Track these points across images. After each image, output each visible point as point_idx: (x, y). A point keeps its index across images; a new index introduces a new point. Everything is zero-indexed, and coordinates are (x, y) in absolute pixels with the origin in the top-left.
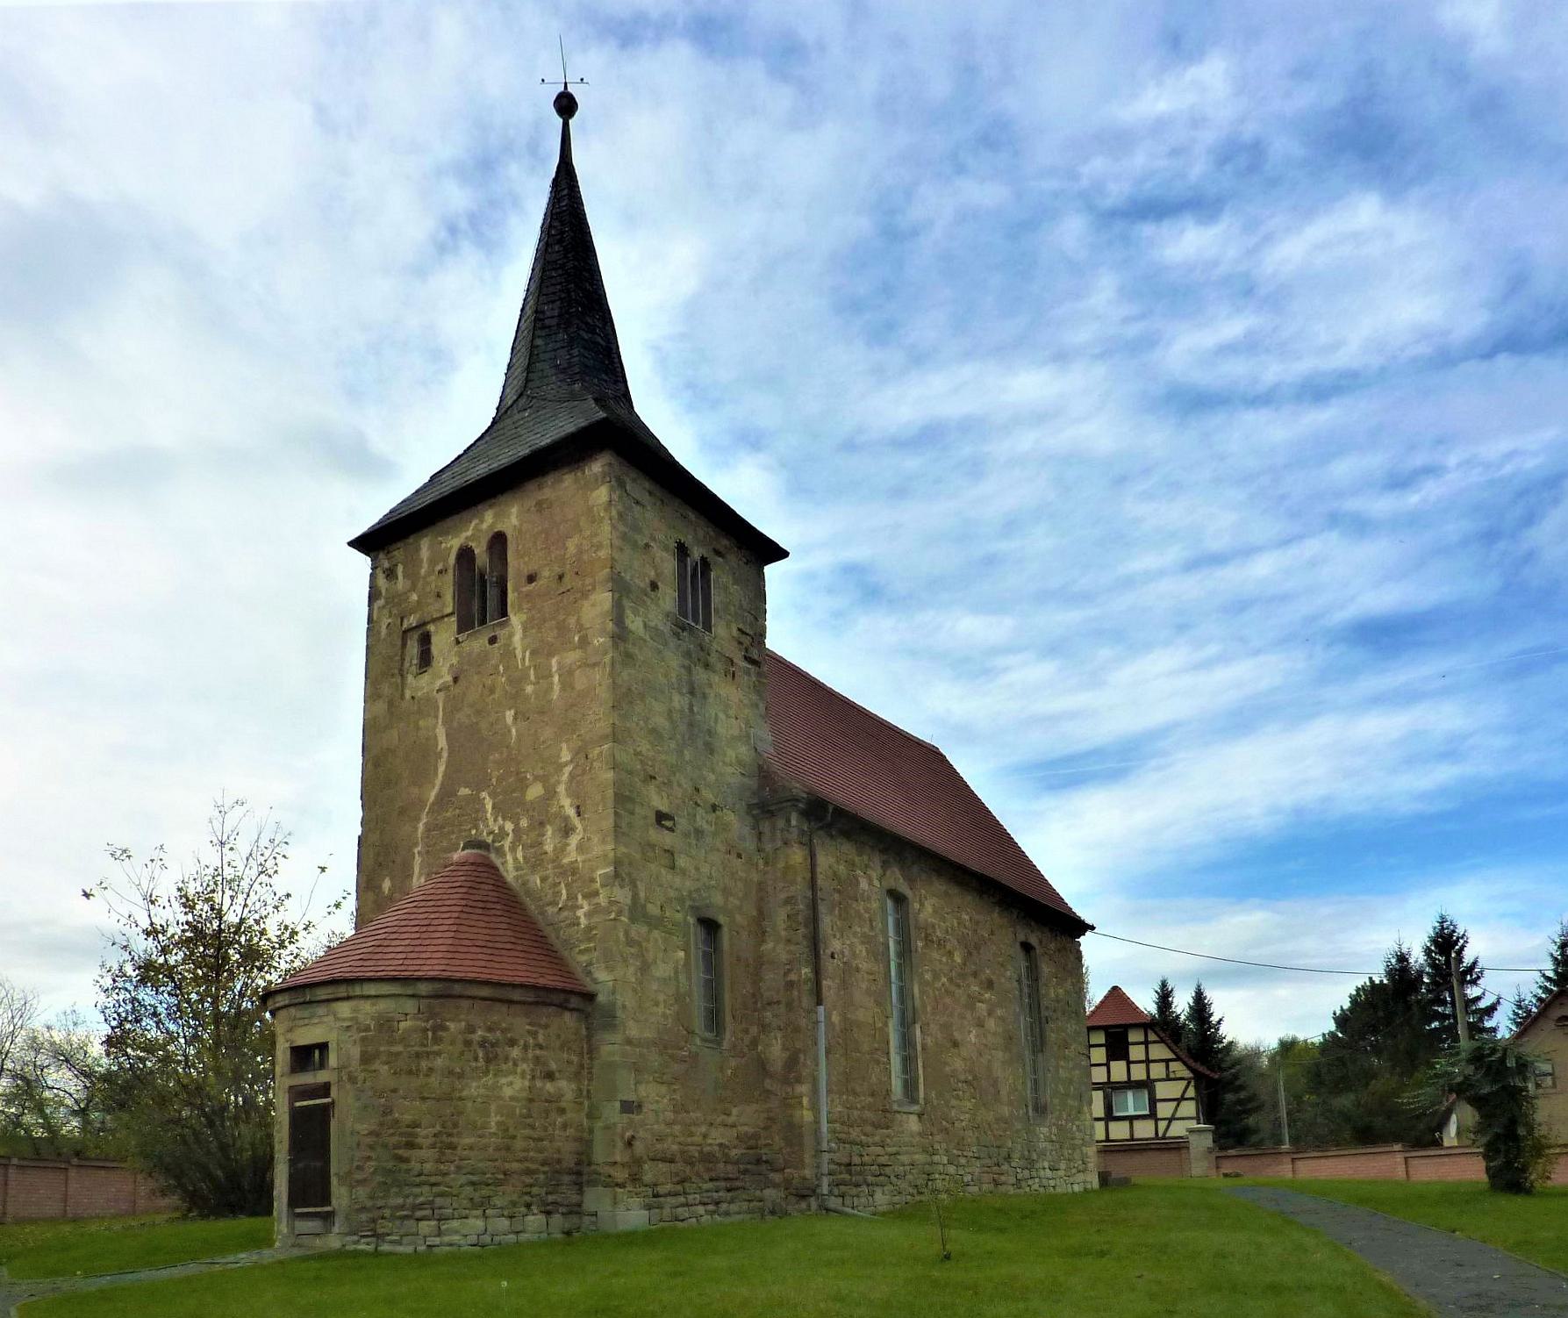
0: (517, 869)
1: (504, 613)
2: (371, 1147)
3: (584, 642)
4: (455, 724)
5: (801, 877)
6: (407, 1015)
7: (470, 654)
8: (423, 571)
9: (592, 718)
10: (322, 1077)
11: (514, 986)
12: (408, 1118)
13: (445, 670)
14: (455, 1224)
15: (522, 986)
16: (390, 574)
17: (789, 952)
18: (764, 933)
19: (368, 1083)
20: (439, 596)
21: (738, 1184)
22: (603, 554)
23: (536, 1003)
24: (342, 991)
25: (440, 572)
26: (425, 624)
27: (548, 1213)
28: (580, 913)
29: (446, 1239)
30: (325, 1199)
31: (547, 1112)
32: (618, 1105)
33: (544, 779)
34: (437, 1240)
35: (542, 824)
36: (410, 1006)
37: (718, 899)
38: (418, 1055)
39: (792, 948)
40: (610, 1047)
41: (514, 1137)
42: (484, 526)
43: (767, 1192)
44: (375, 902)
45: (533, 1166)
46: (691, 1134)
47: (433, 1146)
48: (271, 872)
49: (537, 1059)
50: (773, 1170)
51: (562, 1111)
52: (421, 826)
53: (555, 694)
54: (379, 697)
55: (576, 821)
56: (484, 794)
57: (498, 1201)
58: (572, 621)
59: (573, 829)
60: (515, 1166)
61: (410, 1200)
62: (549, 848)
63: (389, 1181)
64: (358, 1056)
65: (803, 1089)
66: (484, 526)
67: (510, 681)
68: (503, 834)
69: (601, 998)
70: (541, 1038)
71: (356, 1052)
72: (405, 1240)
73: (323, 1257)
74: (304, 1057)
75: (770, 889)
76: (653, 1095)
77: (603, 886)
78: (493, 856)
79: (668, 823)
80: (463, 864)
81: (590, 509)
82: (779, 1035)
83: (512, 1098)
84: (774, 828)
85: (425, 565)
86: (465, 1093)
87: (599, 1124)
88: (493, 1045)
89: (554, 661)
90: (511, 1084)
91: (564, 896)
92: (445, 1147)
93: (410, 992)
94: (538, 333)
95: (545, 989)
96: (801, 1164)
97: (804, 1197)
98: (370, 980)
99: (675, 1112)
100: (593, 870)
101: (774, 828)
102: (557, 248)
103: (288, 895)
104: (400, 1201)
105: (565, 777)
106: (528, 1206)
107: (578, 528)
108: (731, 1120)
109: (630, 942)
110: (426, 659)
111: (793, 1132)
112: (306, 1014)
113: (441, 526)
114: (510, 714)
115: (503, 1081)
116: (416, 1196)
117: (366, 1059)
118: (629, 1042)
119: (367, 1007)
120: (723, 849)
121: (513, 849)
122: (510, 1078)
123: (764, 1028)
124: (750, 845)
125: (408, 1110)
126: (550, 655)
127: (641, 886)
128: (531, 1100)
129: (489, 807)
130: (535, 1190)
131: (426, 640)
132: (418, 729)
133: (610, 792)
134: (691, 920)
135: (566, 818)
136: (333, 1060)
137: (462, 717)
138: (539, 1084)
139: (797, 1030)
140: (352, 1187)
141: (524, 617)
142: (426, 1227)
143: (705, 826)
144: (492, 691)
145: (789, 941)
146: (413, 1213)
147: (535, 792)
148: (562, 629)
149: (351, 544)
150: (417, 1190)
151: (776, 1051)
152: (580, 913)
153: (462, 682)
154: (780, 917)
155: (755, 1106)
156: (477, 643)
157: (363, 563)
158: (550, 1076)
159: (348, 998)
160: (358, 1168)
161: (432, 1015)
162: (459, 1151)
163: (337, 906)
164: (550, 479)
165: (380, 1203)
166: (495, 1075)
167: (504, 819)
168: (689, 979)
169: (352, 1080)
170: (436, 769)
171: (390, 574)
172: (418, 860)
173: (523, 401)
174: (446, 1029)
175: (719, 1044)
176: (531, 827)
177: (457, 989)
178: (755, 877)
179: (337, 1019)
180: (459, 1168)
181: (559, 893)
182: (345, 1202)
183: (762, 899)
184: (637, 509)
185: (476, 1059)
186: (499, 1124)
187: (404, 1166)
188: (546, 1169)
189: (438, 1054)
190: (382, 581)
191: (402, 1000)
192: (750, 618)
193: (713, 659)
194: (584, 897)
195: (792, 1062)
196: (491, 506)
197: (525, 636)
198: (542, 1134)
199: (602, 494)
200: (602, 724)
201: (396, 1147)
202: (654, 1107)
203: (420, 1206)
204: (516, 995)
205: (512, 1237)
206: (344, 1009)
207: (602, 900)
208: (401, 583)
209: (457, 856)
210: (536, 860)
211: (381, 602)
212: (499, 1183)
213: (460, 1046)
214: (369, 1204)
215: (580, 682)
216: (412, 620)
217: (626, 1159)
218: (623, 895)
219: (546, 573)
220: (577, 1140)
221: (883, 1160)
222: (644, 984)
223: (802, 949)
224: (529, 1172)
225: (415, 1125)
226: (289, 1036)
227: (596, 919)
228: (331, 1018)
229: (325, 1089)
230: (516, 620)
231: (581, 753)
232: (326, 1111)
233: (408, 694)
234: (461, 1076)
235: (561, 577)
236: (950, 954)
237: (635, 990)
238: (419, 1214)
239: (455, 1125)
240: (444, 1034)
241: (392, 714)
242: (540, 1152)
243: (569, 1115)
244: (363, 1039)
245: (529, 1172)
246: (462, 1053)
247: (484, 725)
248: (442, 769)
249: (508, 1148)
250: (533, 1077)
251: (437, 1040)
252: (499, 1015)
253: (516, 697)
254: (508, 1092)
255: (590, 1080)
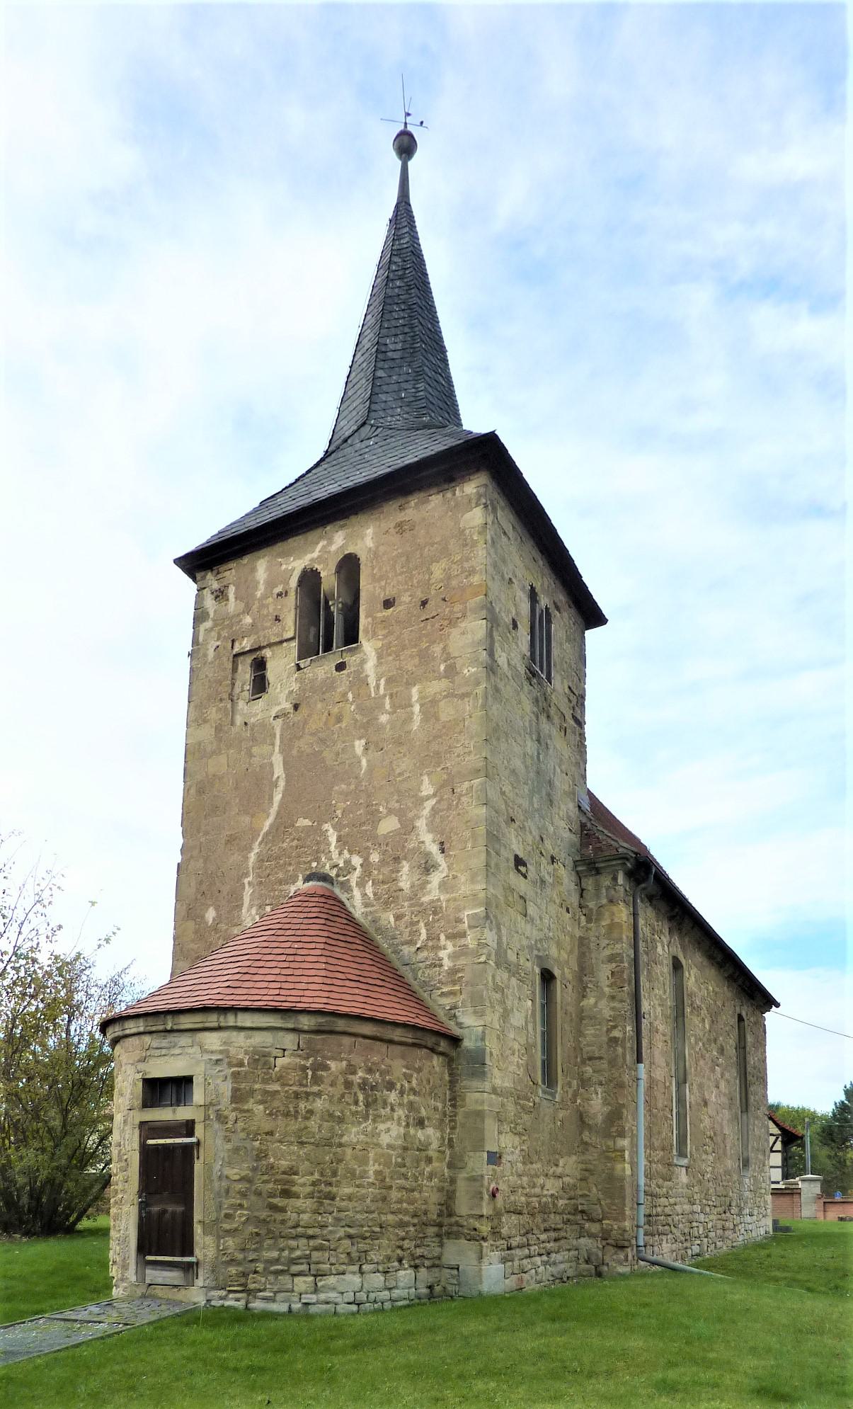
0: (366, 905)
1: (351, 637)
2: (243, 1195)
3: (451, 672)
4: (295, 752)
5: (627, 934)
6: (284, 1049)
7: (312, 681)
8: (259, 594)
9: (460, 750)
10: (183, 1113)
11: (395, 1024)
12: (284, 1163)
13: (283, 696)
14: (332, 1280)
15: (404, 1026)
16: (220, 595)
17: (613, 1009)
18: (585, 988)
19: (240, 1124)
20: (277, 619)
21: (563, 1234)
22: (476, 579)
23: (414, 1045)
24: (212, 1020)
25: (279, 595)
26: (260, 648)
27: (416, 1267)
28: (443, 954)
29: (322, 1296)
30: (188, 1249)
31: (418, 1161)
32: (485, 1155)
33: (401, 814)
34: (313, 1298)
35: (397, 860)
36: (289, 1040)
37: (554, 952)
38: (297, 1095)
39: (616, 1004)
40: (477, 1096)
41: (391, 1187)
42: (333, 548)
43: (582, 1241)
44: (196, 932)
45: (406, 1218)
46: (534, 1186)
47: (310, 1195)
48: (46, 902)
49: (411, 1104)
50: (592, 1220)
51: (429, 1160)
52: (252, 857)
53: (416, 724)
54: (205, 721)
55: (439, 858)
56: (326, 826)
57: (373, 1256)
58: (437, 649)
59: (435, 866)
60: (391, 1218)
61: (286, 1253)
62: (405, 883)
63: (263, 1232)
64: (229, 1094)
65: (625, 1143)
66: (333, 548)
67: (360, 709)
68: (349, 868)
69: (468, 1044)
70: (414, 1082)
71: (226, 1088)
72: (280, 1296)
73: (190, 1317)
74: (160, 1090)
75: (592, 946)
76: (507, 1143)
77: (470, 927)
78: (337, 891)
79: (523, 869)
80: (312, 895)
81: (462, 532)
82: (599, 1090)
83: (390, 1146)
84: (598, 888)
85: (262, 587)
86: (345, 1139)
87: (463, 1175)
88: (373, 1088)
89: (415, 691)
90: (388, 1130)
91: (424, 936)
92: (324, 1197)
93: (290, 1026)
94: (380, 364)
95: (423, 1029)
96: (621, 1216)
97: (623, 1247)
98: (246, 1010)
99: (524, 1163)
100: (459, 910)
101: (598, 888)
102: (398, 283)
103: (60, 927)
104: (275, 1254)
105: (426, 812)
106: (400, 1261)
107: (445, 552)
108: (559, 1170)
109: (498, 989)
110: (260, 685)
111: (614, 1186)
112: (164, 1043)
113: (279, 547)
114: (359, 745)
115: (382, 1127)
116: (292, 1249)
117: (238, 1097)
118: (494, 1091)
119: (239, 1039)
120: (558, 901)
121: (361, 884)
122: (388, 1124)
123: (584, 1083)
124: (574, 900)
125: (284, 1156)
126: (410, 684)
127: (504, 931)
128: (405, 1149)
129: (333, 839)
130: (406, 1244)
131: (260, 665)
132: (251, 756)
133: (482, 830)
134: (537, 970)
135: (428, 855)
136: (198, 1095)
137: (303, 744)
138: (412, 1131)
139: (621, 1086)
140: (219, 1237)
141: (380, 644)
142: (302, 1283)
143: (547, 877)
144: (339, 719)
145: (613, 998)
146: (287, 1269)
147: (388, 825)
148: (425, 657)
149: (178, 562)
150: (293, 1243)
151: (597, 1105)
152: (443, 954)
153: (303, 710)
154: (604, 973)
155: (574, 1158)
156: (322, 668)
157: (186, 587)
158: (421, 1123)
159: (219, 1029)
160: (227, 1216)
161: (312, 1051)
162: (337, 1202)
163: (107, 940)
164: (413, 500)
165: (252, 1256)
166: (374, 1121)
167: (351, 852)
168: (534, 1029)
169: (221, 1118)
170: (271, 798)
171: (220, 595)
172: (248, 891)
173: (366, 431)
174: (326, 1068)
175: (553, 1095)
176: (383, 862)
177: (341, 1025)
178: (578, 933)
179: (204, 1051)
180: (338, 1220)
181: (418, 932)
182: (211, 1253)
183: (584, 953)
184: (504, 539)
185: (356, 1103)
186: (377, 1173)
187: (279, 1217)
188: (416, 1221)
189: (319, 1094)
190: (210, 603)
191: (281, 1034)
192: (576, 679)
193: (553, 711)
194: (448, 938)
195: (615, 1116)
196: (342, 527)
197: (379, 664)
198: (414, 1184)
199: (476, 516)
200: (472, 757)
201: (272, 1195)
202: (510, 1158)
203: (294, 1261)
204: (397, 1035)
205: (385, 1295)
206: (213, 1040)
207: (470, 941)
208: (232, 605)
209: (300, 885)
210: (390, 898)
211: (208, 624)
212: (374, 1236)
213: (340, 1088)
214: (240, 1256)
215: (446, 712)
216: (246, 644)
217: (491, 1212)
218: (490, 937)
219: (406, 598)
220: (441, 1190)
221: (667, 1210)
222: (501, 1029)
223: (626, 1007)
224: (402, 1225)
225: (293, 1171)
226: (141, 1066)
227: (462, 961)
228: (196, 1049)
229: (188, 1128)
230: (368, 646)
231: (448, 786)
232: (188, 1153)
233: (239, 720)
234: (341, 1120)
235: (424, 603)
236: (703, 1020)
237: (498, 1038)
238: (295, 1269)
239: (335, 1174)
240: (324, 1074)
241: (220, 740)
242: (411, 1203)
243: (435, 1164)
244: (236, 1075)
245: (402, 1225)
246: (343, 1096)
247: (328, 755)
248: (278, 797)
249: (384, 1199)
250: (408, 1125)
251: (317, 1080)
252: (378, 1054)
253: (367, 726)
254: (385, 1139)
255: (453, 1128)
